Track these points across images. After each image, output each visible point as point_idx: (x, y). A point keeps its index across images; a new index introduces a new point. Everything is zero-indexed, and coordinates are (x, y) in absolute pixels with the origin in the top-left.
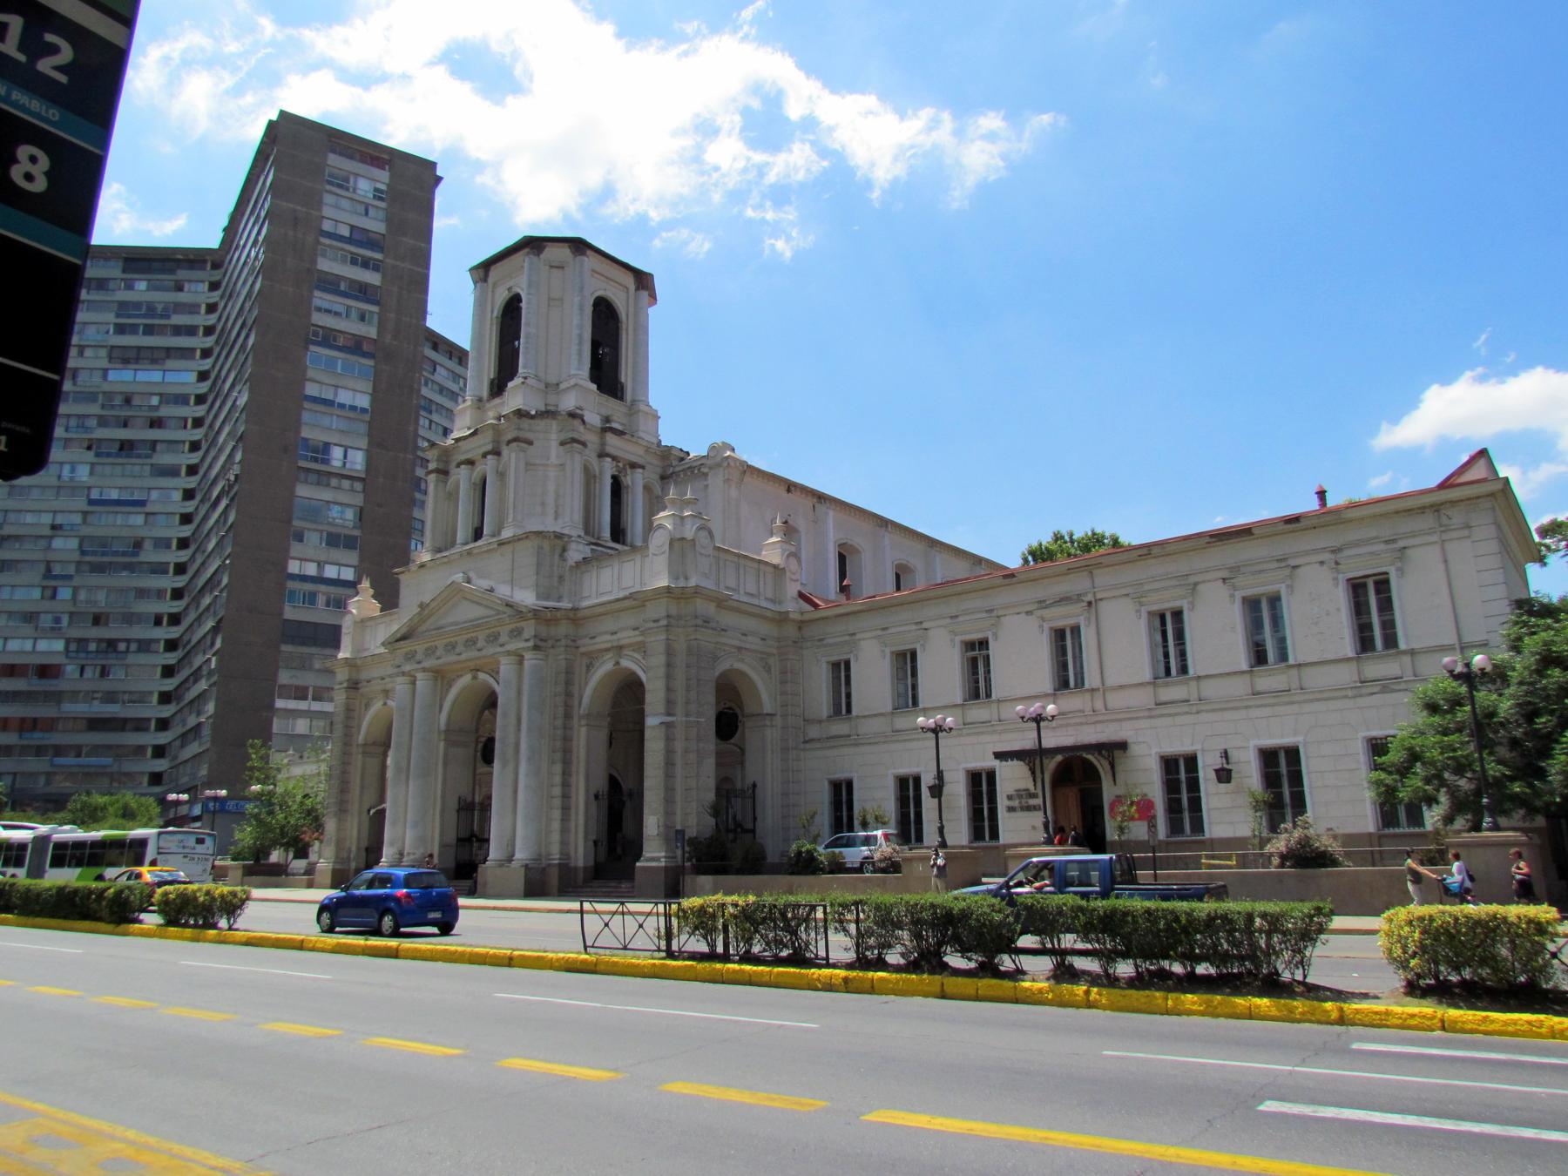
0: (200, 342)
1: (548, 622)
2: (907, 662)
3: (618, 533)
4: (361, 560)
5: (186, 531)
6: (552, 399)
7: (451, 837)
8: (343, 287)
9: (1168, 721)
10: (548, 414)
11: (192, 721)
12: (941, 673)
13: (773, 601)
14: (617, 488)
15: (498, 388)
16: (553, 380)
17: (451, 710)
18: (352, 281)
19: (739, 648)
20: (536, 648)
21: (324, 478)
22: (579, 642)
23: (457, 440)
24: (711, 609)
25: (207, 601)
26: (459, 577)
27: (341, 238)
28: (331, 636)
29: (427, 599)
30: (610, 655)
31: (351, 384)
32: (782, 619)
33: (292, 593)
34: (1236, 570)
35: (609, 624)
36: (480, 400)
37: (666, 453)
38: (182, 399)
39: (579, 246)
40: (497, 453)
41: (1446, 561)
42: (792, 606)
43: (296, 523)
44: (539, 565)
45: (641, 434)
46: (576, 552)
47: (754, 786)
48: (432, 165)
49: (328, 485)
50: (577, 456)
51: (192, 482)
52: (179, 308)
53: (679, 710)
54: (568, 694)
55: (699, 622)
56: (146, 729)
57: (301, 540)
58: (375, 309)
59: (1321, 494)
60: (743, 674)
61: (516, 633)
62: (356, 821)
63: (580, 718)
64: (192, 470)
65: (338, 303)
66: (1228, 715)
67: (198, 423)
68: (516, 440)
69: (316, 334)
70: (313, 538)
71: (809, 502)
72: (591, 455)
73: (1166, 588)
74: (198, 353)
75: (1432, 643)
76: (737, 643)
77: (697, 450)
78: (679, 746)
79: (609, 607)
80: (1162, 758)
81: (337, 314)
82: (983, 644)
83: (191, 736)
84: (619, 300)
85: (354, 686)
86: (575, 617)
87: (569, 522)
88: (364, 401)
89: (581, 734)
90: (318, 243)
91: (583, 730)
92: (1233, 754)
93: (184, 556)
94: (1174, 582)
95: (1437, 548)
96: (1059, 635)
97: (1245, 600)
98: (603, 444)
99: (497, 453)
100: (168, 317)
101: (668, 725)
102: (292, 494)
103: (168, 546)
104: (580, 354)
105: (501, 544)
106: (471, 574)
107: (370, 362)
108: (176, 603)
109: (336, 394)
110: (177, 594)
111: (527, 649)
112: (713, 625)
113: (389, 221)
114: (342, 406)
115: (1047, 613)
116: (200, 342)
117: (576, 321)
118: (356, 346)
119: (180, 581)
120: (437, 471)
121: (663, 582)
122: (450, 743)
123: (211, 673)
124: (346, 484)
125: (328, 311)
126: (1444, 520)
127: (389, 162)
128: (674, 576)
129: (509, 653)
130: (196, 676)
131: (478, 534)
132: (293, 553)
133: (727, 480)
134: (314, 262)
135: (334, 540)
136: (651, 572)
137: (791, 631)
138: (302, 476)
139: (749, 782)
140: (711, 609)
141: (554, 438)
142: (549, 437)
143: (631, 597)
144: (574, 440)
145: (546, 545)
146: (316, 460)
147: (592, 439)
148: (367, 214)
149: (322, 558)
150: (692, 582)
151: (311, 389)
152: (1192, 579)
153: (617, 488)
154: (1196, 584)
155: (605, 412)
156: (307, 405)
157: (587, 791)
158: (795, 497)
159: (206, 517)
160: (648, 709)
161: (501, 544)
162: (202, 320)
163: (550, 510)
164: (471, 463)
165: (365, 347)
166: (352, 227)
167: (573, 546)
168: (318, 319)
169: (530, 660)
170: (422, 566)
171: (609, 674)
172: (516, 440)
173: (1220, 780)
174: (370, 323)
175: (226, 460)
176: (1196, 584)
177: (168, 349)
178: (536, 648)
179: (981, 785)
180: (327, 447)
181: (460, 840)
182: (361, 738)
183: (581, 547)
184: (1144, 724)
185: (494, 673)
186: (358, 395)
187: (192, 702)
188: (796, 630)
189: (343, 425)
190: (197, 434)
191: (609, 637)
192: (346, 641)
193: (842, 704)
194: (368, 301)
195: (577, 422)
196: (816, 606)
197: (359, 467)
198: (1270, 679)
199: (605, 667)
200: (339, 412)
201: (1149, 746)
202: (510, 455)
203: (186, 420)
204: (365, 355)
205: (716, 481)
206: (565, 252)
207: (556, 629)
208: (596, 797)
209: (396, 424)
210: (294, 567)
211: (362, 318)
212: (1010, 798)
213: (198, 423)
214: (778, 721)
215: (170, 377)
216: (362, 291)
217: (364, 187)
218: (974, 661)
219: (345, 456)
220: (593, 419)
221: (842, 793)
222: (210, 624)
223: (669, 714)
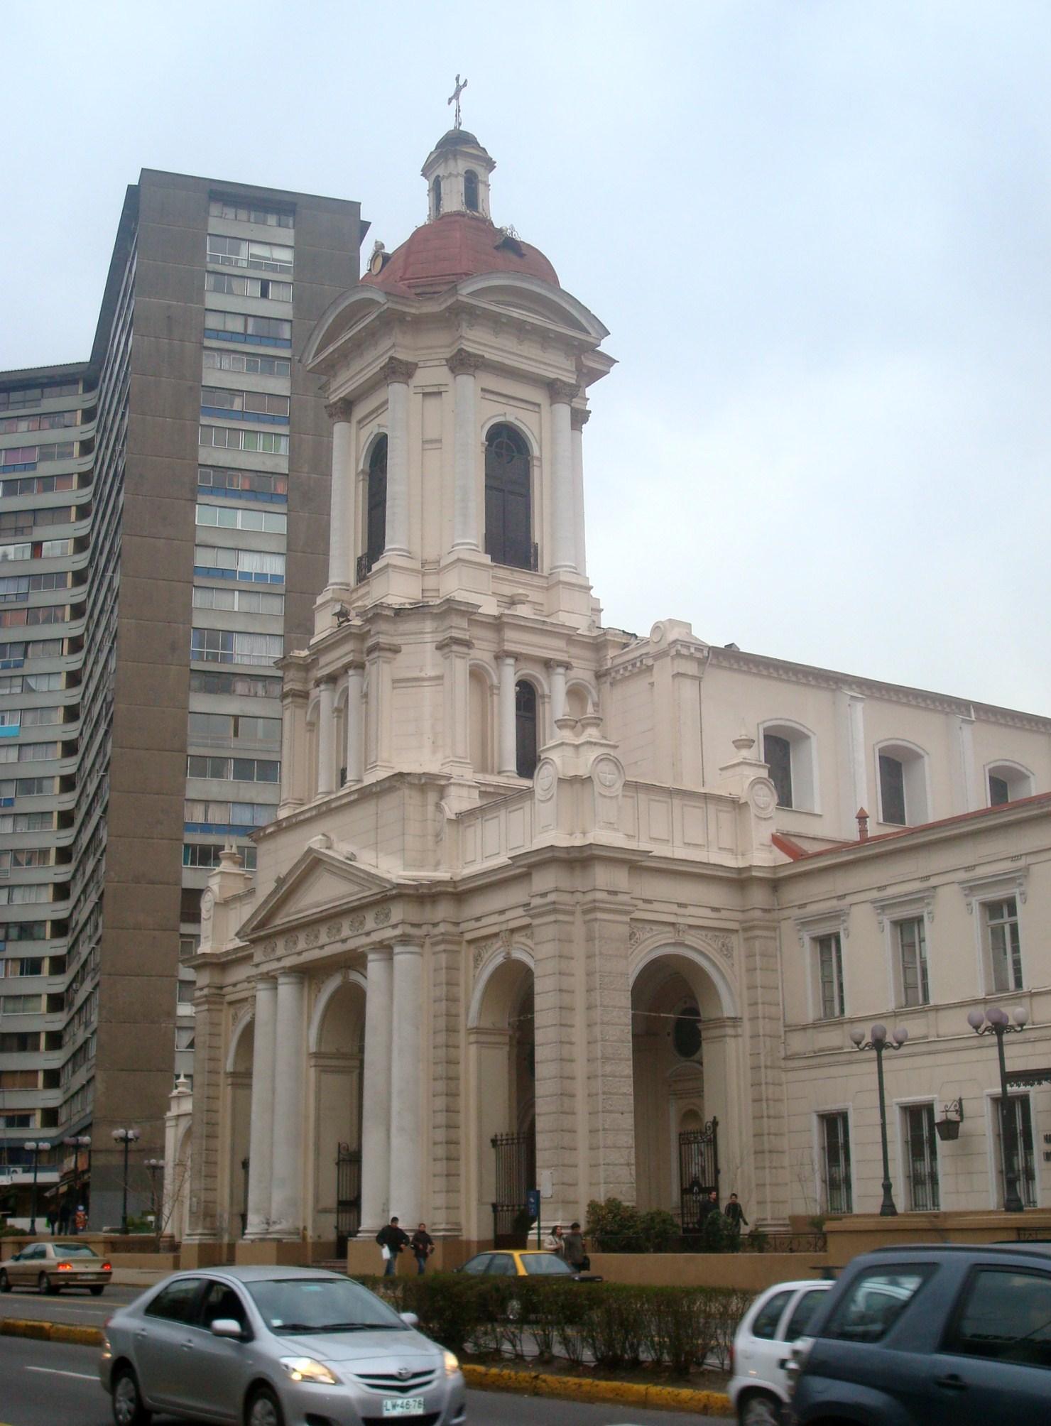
7: (330, 1201)
14: (528, 698)
15: (365, 566)
16: (431, 554)
37: (599, 643)
46: (458, 801)
47: (715, 1123)
48: (352, 208)
56: (36, 1048)
72: (483, 653)
83: (80, 1056)
84: (525, 421)
99: (360, 666)
100: (33, 466)
114: (246, 575)
116: (75, 496)
122: (323, 1070)
132: (190, 794)
134: (199, 378)
139: (708, 1118)
146: (214, 657)
148: (264, 294)
153: (528, 698)
155: (508, 590)
157: (480, 1138)
177: (35, 511)
186: (268, 558)
205: (663, 673)
214: (746, 1028)
218: (997, 934)
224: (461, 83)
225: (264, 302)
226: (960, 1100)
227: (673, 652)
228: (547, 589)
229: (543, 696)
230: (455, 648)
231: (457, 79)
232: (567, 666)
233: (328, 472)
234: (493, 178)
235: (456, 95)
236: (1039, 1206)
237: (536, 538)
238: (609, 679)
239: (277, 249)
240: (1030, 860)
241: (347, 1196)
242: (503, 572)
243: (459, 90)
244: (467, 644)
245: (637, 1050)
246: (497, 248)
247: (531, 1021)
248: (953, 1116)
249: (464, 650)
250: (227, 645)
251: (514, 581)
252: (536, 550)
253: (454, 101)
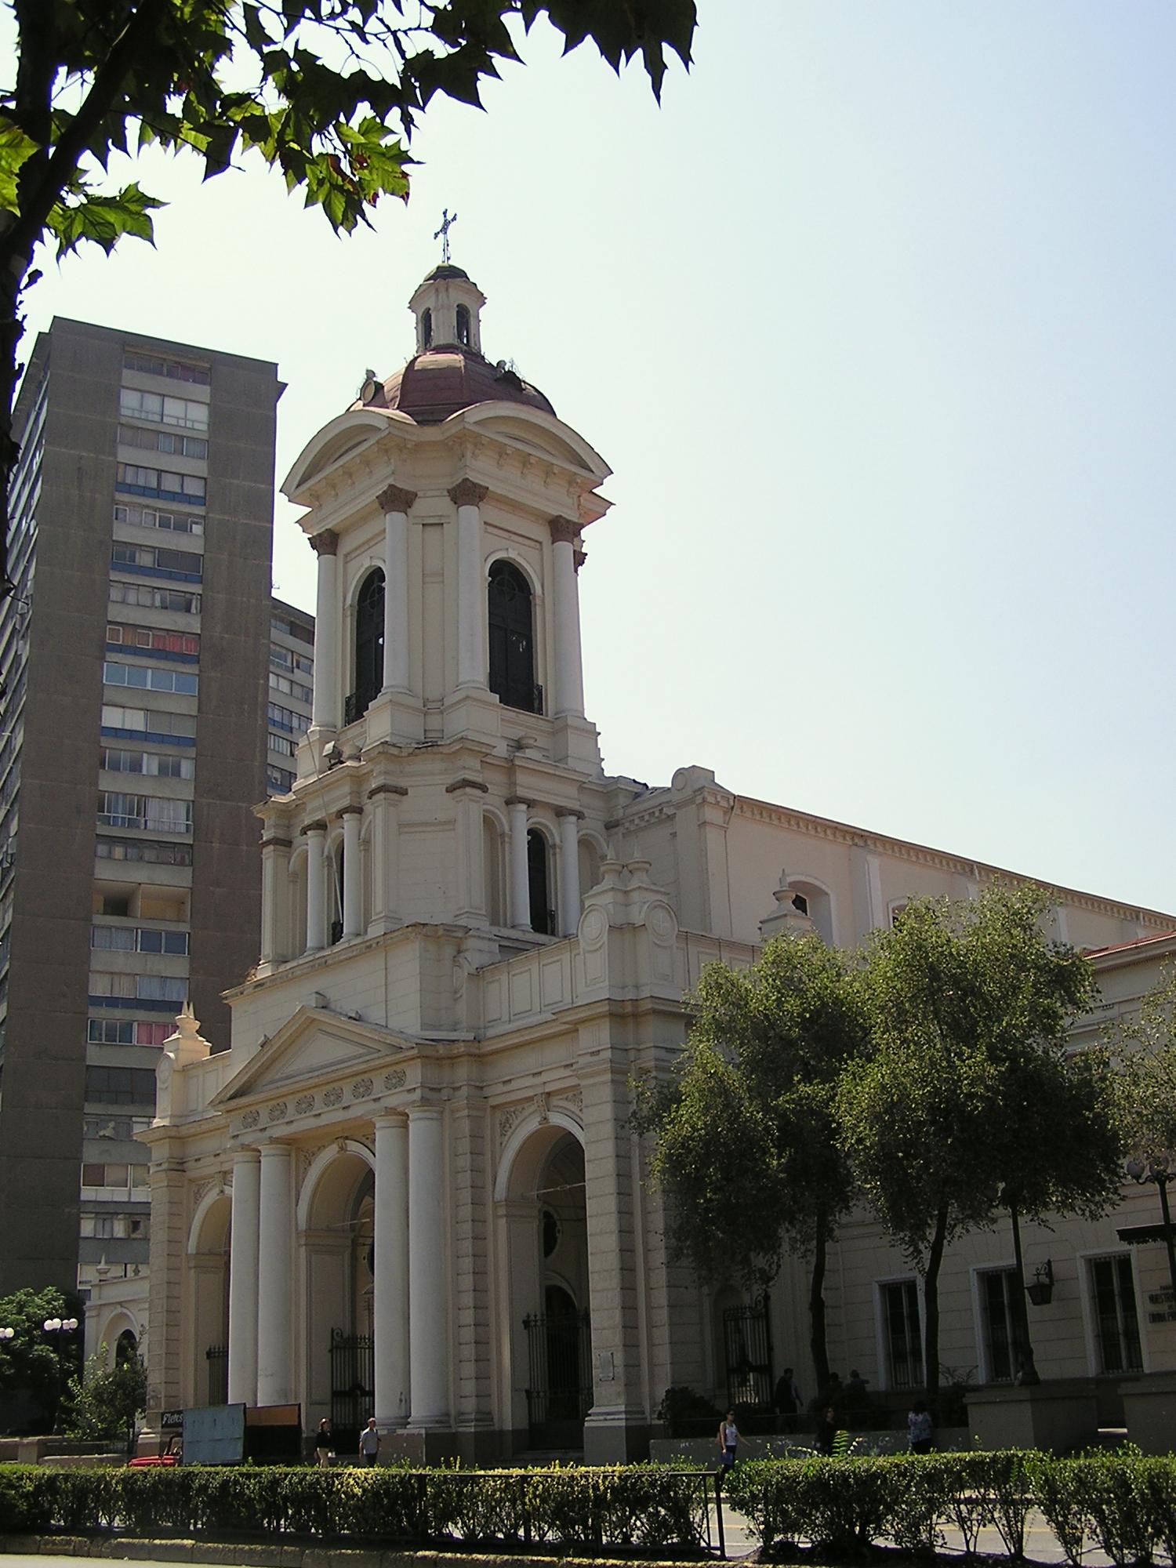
3: (543, 919)
4: (192, 970)
6: (434, 722)
7: (324, 1392)
10: (428, 745)
15: (356, 709)
20: (425, 1101)
22: (487, 1092)
28: (138, 1089)
35: (530, 1060)
40: (359, 811)
49: (141, 859)
61: (396, 1080)
63: (496, 1204)
72: (494, 800)
77: (659, 778)
85: (179, 1166)
99: (359, 811)
107: (193, 669)
131: (336, 932)
136: (576, 973)
138: (102, 849)
144: (467, 783)
153: (538, 845)
155: (516, 733)
157: (512, 1318)
170: (260, 985)
181: (336, 1394)
185: (369, 1142)
191: (530, 1081)
192: (164, 1102)
199: (528, 1126)
202: (377, 810)
207: (454, 1065)
208: (526, 1324)
209: (234, 751)
212: (1154, 1299)
224: (449, 217)
225: (176, 459)
226: (1049, 1262)
227: (699, 800)
228: (553, 734)
229: (554, 846)
230: (468, 790)
231: (445, 213)
232: (580, 816)
234: (483, 312)
235: (444, 229)
236: (1147, 1370)
238: (620, 830)
239: (189, 413)
240: (1124, 1008)
242: (512, 713)
243: (446, 224)
244: (483, 788)
246: (497, 380)
247: (583, 1189)
248: (1045, 1280)
249: (478, 792)
250: (142, 810)
251: (521, 722)
252: (540, 693)
253: (441, 235)
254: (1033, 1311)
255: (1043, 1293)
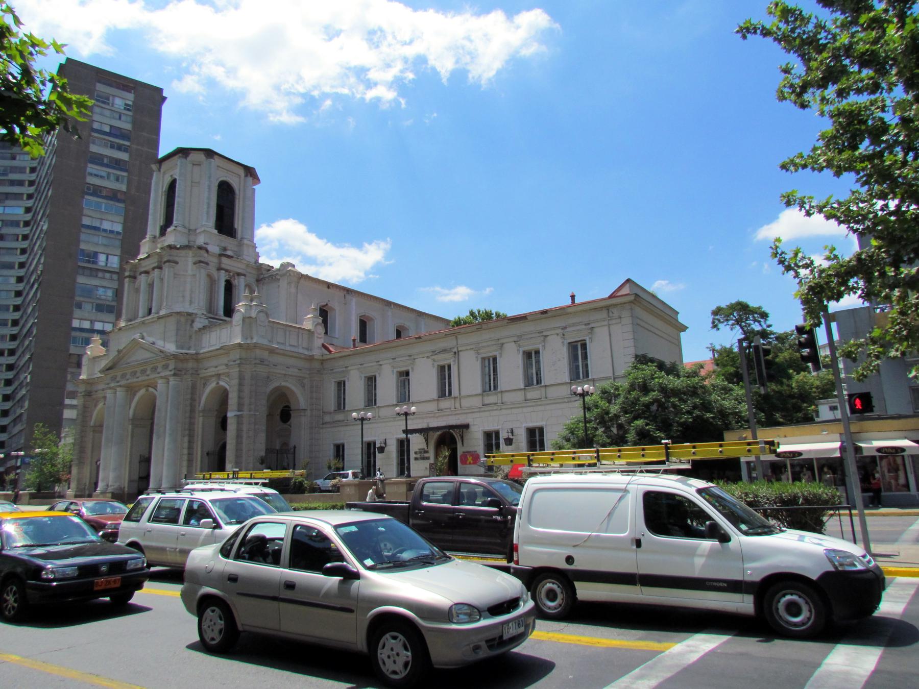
0: (27, 190)
1: (182, 361)
2: (371, 381)
5: (19, 301)
7: (136, 477)
8: (105, 161)
9: (487, 414)
10: (187, 247)
11: (19, 411)
12: (387, 389)
13: (307, 349)
14: (229, 288)
15: (163, 231)
16: (193, 227)
17: (136, 407)
18: (110, 158)
19: (285, 375)
20: (175, 375)
21: (94, 272)
23: (140, 260)
24: (265, 355)
25: (27, 343)
26: (137, 336)
27: (105, 133)
29: (121, 348)
30: (213, 379)
31: (110, 218)
32: (311, 359)
33: (75, 338)
34: (520, 337)
36: (155, 237)
38: (16, 224)
39: (209, 153)
41: (610, 335)
42: (317, 352)
43: (77, 299)
44: (178, 330)
45: (245, 257)
46: (198, 325)
47: (295, 447)
48: (160, 90)
50: (203, 270)
51: (22, 272)
52: (14, 170)
53: (246, 408)
54: (193, 399)
55: (258, 362)
57: (80, 308)
58: (125, 174)
59: (573, 297)
60: (288, 388)
61: (166, 367)
62: (89, 467)
64: (22, 265)
65: (103, 171)
66: (514, 411)
67: (25, 237)
68: (168, 261)
69: (89, 189)
70: (87, 307)
71: (342, 293)
73: (488, 346)
74: (25, 196)
75: (602, 376)
76: (284, 372)
78: (245, 428)
79: (213, 354)
80: (398, 440)
81: (102, 177)
82: (407, 374)
84: (234, 182)
85: (88, 394)
86: (197, 358)
87: (198, 306)
88: (119, 228)
89: (199, 421)
90: (91, 135)
91: (201, 419)
92: (515, 432)
93: (16, 315)
94: (493, 343)
95: (606, 328)
96: (442, 368)
97: (524, 352)
98: (220, 263)
99: (160, 268)
101: (238, 416)
102: (75, 281)
103: (8, 310)
104: (208, 213)
105: (159, 318)
106: (145, 334)
107: (122, 205)
108: (12, 343)
109: (101, 224)
110: (13, 338)
111: (170, 375)
112: (266, 363)
113: (134, 123)
114: (105, 230)
115: (435, 357)
116: (27, 190)
117: (206, 194)
118: (114, 196)
119: (15, 330)
120: (129, 277)
121: (238, 340)
123: (27, 384)
124: (108, 275)
125: (96, 175)
126: (611, 314)
127: (134, 88)
128: (244, 337)
129: (162, 378)
130: (21, 385)
132: (75, 316)
133: (289, 283)
134: (88, 147)
135: (100, 308)
136: (232, 334)
137: (317, 365)
138: (81, 271)
140: (265, 355)
141: (190, 261)
142: (187, 260)
143: (221, 348)
144: (200, 262)
145: (183, 319)
146: (89, 262)
147: (213, 261)
148: (120, 118)
149: (94, 318)
150: (254, 341)
151: (86, 221)
152: (501, 341)
153: (229, 288)
154: (503, 344)
155: (223, 245)
156: (83, 230)
157: (202, 451)
158: (331, 291)
159: (28, 294)
160: (230, 408)
161: (159, 318)
162: (27, 176)
163: (188, 298)
164: (147, 272)
165: (119, 196)
166: (111, 126)
167: (198, 319)
168: (90, 180)
169: (173, 381)
170: (120, 329)
171: (213, 392)
172: (168, 261)
173: (511, 444)
174: (122, 182)
175: (37, 262)
176: (503, 344)
178: (175, 375)
179: (403, 446)
180: (95, 255)
181: (140, 478)
182: (92, 423)
183: (202, 320)
184: (477, 415)
185: (155, 388)
187: (19, 401)
188: (318, 367)
189: (105, 241)
190: (25, 244)
191: (214, 369)
192: (84, 369)
193: (341, 404)
194: (121, 170)
195: (203, 252)
196: (330, 351)
197: (115, 266)
198: (533, 393)
200: (105, 234)
201: (479, 425)
203: (18, 236)
204: (119, 201)
205: (283, 283)
206: (201, 157)
207: (186, 365)
208: (208, 454)
210: (76, 323)
211: (117, 179)
212: (416, 453)
213: (25, 237)
215: (8, 211)
216: (117, 164)
217: (119, 103)
219: (107, 259)
220: (214, 249)
221: (339, 450)
222: (28, 356)
223: (239, 411)
225: (119, 122)
233: (148, 193)
237: (236, 226)
241: (143, 475)
242: (223, 237)
244: (207, 264)
245: (268, 420)
248: (383, 445)
254: (378, 455)
255: (382, 450)
